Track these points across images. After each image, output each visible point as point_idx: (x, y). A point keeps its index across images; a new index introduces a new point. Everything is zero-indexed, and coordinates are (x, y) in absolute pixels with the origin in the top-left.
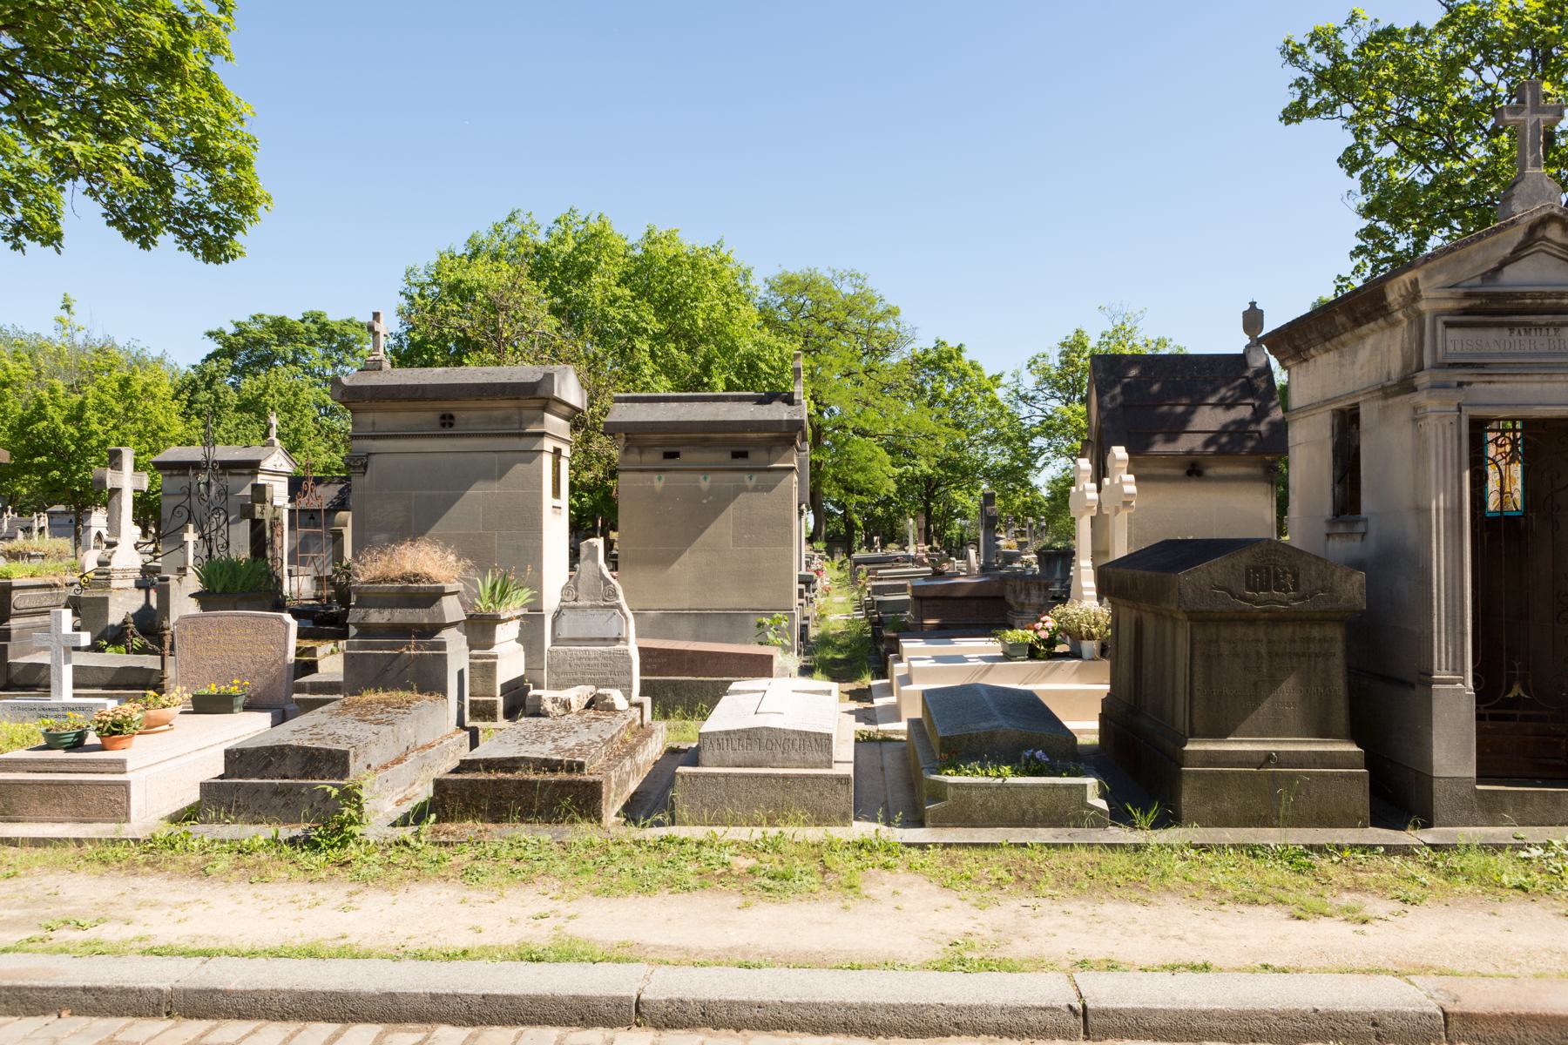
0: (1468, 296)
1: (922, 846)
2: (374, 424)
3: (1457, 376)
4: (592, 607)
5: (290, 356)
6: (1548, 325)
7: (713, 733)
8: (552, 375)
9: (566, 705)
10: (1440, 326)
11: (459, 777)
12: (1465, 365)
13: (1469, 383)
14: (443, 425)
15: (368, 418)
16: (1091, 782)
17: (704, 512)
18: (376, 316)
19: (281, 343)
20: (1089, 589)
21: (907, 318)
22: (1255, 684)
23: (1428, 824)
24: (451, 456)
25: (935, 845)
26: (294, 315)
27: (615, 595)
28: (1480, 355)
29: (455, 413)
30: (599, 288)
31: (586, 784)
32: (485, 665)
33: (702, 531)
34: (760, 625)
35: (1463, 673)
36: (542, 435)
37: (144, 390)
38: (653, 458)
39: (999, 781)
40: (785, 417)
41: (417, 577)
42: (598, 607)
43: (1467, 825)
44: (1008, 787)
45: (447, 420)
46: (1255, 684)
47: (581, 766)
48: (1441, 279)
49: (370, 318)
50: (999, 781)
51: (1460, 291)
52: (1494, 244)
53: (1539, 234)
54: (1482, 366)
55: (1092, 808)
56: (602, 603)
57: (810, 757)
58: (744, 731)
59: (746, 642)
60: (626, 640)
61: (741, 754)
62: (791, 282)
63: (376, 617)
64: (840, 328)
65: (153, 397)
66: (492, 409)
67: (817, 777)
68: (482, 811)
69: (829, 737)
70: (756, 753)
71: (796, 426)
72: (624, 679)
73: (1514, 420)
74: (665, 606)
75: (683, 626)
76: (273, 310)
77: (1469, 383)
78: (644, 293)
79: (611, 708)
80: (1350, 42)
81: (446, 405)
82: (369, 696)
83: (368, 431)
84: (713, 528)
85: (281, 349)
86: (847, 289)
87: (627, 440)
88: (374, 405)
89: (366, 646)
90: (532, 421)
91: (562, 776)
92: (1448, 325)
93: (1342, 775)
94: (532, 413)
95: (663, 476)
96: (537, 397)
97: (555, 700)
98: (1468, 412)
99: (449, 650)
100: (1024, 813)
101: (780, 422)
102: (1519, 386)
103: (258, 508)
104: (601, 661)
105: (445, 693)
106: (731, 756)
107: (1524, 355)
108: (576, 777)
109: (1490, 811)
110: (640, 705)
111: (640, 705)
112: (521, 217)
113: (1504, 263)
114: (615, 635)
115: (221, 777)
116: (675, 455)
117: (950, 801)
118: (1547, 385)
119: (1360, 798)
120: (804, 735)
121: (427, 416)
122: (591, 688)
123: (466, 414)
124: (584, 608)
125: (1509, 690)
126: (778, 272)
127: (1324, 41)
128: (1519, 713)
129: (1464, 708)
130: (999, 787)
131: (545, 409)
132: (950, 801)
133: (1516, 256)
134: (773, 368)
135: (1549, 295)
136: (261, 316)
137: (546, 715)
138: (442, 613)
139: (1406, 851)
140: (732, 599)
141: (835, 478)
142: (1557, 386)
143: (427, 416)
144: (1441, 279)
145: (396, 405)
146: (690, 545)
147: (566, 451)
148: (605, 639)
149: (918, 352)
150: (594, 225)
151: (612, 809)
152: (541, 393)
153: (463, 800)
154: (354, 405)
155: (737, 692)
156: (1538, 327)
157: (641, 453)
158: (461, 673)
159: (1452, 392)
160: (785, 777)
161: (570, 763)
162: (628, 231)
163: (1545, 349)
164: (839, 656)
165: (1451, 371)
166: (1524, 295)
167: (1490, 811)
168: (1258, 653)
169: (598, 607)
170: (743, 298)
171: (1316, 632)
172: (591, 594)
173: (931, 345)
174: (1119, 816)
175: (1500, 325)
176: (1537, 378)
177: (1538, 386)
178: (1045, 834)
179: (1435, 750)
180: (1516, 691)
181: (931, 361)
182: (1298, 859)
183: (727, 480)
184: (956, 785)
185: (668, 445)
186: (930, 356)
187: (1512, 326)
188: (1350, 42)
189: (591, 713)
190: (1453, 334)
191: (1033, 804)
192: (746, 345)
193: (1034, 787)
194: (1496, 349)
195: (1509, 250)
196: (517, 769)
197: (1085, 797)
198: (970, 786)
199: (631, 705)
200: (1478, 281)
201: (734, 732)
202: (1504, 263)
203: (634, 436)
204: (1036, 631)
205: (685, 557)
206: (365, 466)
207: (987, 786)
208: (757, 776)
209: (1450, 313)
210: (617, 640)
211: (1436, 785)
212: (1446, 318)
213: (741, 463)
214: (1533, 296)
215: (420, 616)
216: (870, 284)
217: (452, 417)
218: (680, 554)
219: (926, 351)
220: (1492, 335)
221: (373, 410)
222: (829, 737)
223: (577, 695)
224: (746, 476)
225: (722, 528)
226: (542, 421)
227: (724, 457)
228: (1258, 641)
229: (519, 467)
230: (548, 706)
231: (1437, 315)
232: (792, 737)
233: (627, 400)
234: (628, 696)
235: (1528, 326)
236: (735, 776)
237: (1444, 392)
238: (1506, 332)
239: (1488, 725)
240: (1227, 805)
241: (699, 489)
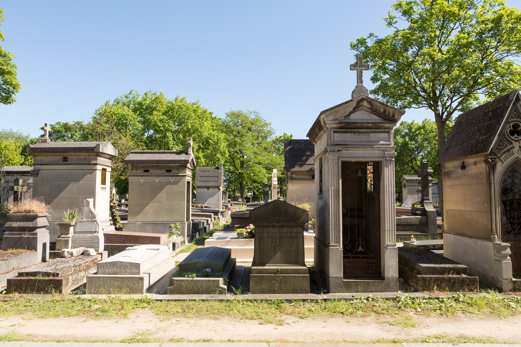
0: (340, 123)
1: (161, 301)
2: (41, 160)
3: (337, 148)
4: (87, 221)
5: (70, 136)
6: (365, 132)
8: (99, 145)
9: (72, 254)
10: (332, 132)
11: (18, 278)
12: (340, 145)
13: (341, 150)
14: (64, 161)
15: (39, 158)
16: (221, 280)
17: (156, 190)
18: (46, 125)
19: (66, 132)
21: (274, 126)
22: (275, 247)
23: (328, 292)
24: (66, 171)
25: (165, 300)
26: (71, 123)
28: (344, 142)
29: (68, 157)
30: (156, 117)
31: (57, 280)
32: (65, 240)
33: (156, 196)
34: (171, 227)
35: (339, 243)
36: (96, 164)
37: (5, 147)
38: (140, 172)
39: (191, 279)
40: (183, 159)
41: (29, 211)
42: (89, 221)
43: (387, 292)
44: (194, 281)
45: (65, 159)
46: (275, 247)
47: (58, 275)
48: (331, 117)
49: (44, 125)
50: (191, 279)
51: (337, 121)
52: (347, 107)
53: (361, 104)
54: (345, 145)
55: (221, 288)
56: (90, 220)
57: (133, 271)
60: (98, 232)
61: (110, 270)
62: (234, 114)
63: (15, 224)
64: (250, 129)
65: (8, 149)
66: (80, 155)
67: (132, 278)
68: (22, 290)
69: (139, 264)
70: (115, 270)
71: (187, 162)
72: (97, 245)
73: (371, 162)
74: (143, 220)
75: (149, 227)
76: (63, 121)
77: (341, 150)
78: (171, 117)
79: (89, 255)
80: (370, 43)
81: (65, 154)
82: (10, 251)
83: (39, 162)
84: (159, 195)
85: (66, 134)
86: (253, 117)
87: (132, 166)
88: (41, 154)
89: (11, 234)
90: (93, 160)
91: (51, 278)
92: (335, 132)
93: (301, 277)
94: (95, 157)
95: (144, 178)
96: (95, 152)
97: (68, 252)
98: (341, 159)
99: (38, 236)
100: (199, 289)
101: (181, 160)
102: (356, 151)
103: (16, 187)
104: (89, 239)
105: (36, 250)
106: (107, 271)
107: (357, 142)
108: (56, 278)
109: (348, 288)
111: (101, 254)
112: (133, 92)
113: (351, 113)
114: (94, 231)
115: (17, 277)
116: (148, 171)
117: (175, 286)
118: (365, 151)
119: (307, 284)
120: (131, 264)
121: (59, 158)
123: (72, 157)
124: (84, 222)
125: (358, 248)
126: (230, 111)
127: (362, 42)
128: (361, 256)
129: (339, 254)
130: (191, 281)
131: (98, 156)
132: (175, 286)
133: (355, 110)
134: (214, 142)
135: (365, 123)
136: (59, 123)
137: (64, 257)
138: (37, 223)
139: (317, 302)
140: (165, 218)
141: (248, 177)
142: (369, 151)
143: (59, 158)
144: (331, 117)
145: (48, 154)
146: (152, 200)
147: (109, 169)
149: (278, 137)
150: (158, 94)
151: (67, 289)
152: (96, 151)
153: (16, 286)
154: (34, 154)
155: (129, 249)
156: (362, 133)
157: (136, 170)
158: (44, 245)
159: (335, 153)
160: (122, 278)
161: (54, 273)
162: (169, 97)
163: (365, 140)
165: (335, 147)
166: (357, 123)
167: (347, 288)
168: (276, 237)
170: (205, 119)
171: (294, 230)
172: (87, 217)
173: (282, 135)
174: (230, 290)
175: (351, 132)
176: (362, 149)
177: (362, 151)
178: (204, 296)
179: (330, 268)
180: (360, 249)
181: (282, 140)
182: (278, 304)
183: (164, 179)
184: (177, 280)
185: (146, 167)
186: (281, 138)
187: (354, 133)
188: (370, 43)
190: (336, 135)
191: (202, 287)
192: (205, 134)
193: (202, 281)
194: (349, 140)
195: (352, 109)
196: (37, 275)
197: (219, 284)
198: (182, 281)
200: (343, 118)
201: (108, 263)
202: (351, 113)
203: (135, 164)
204: (246, 229)
205: (150, 205)
206: (38, 174)
207: (187, 281)
208: (113, 277)
209: (336, 128)
210: (95, 232)
211: (330, 279)
212: (334, 130)
213: (169, 174)
214: (360, 123)
215: (30, 224)
216: (260, 115)
217: (67, 158)
218: (148, 203)
219: (280, 137)
220: (349, 135)
221: (41, 156)
222: (139, 264)
223: (76, 251)
224: (170, 178)
225: (163, 195)
226: (96, 159)
227: (163, 172)
228: (276, 233)
229: (88, 175)
230: (66, 254)
231: (332, 128)
233: (135, 153)
234: (97, 250)
235: (359, 133)
236: (106, 277)
237: (332, 153)
238: (353, 134)
239: (346, 260)
240: (264, 287)
241: (155, 182)
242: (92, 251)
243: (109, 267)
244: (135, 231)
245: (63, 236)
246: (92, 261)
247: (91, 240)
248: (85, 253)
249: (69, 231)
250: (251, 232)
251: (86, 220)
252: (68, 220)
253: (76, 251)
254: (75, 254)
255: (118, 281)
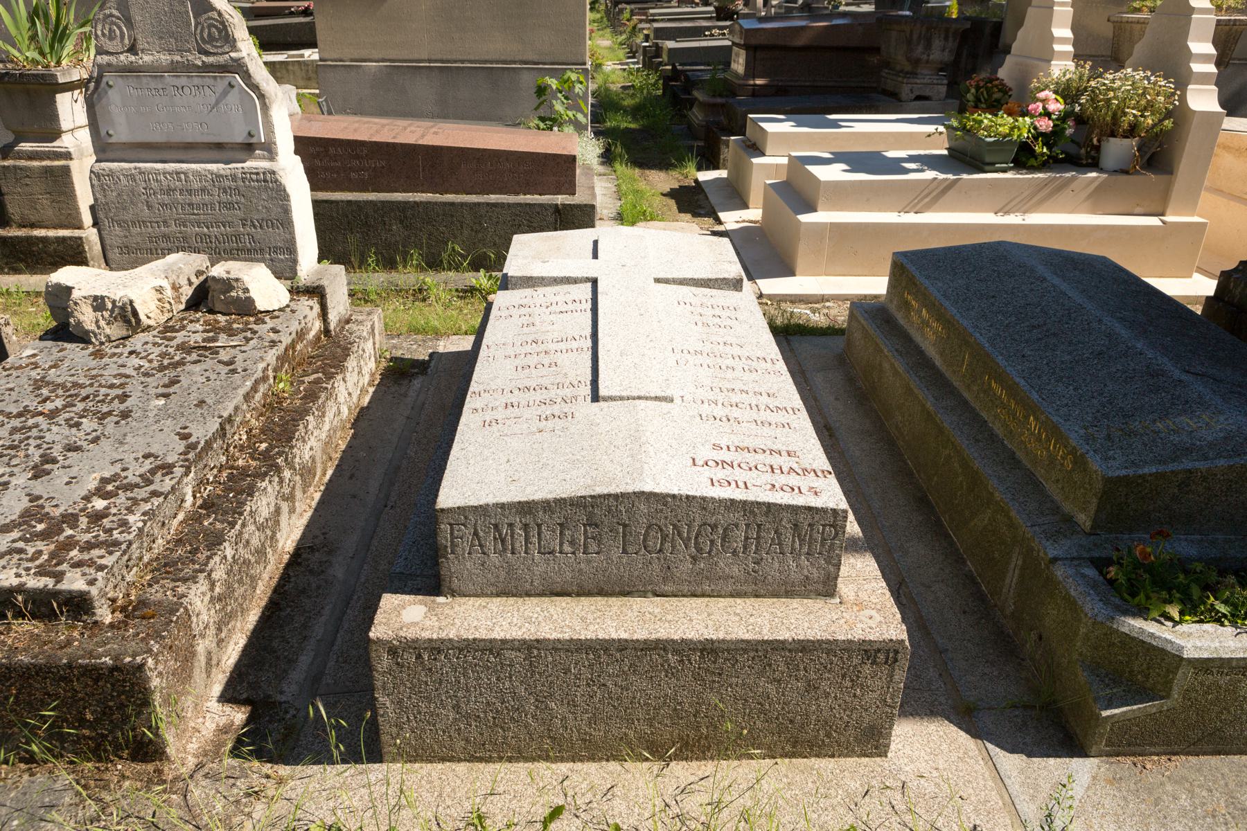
4: (174, 68)
7: (482, 510)
20: (1063, 41)
27: (231, 42)
34: (541, 90)
42: (189, 68)
58: (578, 503)
59: (515, 124)
74: (393, 54)
75: (423, 90)
79: (246, 308)
97: (98, 303)
104: (216, 196)
110: (316, 292)
111: (316, 292)
114: (240, 138)
122: (199, 261)
124: (154, 70)
140: (493, 45)
148: (219, 146)
151: (199, 717)
164: (633, 126)
169: (189, 68)
172: (170, 36)
189: (195, 331)
199: (295, 291)
210: (249, 148)
232: (723, 519)
234: (285, 269)
242: (262, 285)
243: (551, 539)
244: (359, 111)
245: (26, 146)
246: (282, 359)
247: (229, 206)
248: (219, 299)
249: (54, 117)
250: (1057, 132)
251: (165, 58)
252: (32, 54)
253: (150, 286)
254: (148, 309)
255: (670, 672)
